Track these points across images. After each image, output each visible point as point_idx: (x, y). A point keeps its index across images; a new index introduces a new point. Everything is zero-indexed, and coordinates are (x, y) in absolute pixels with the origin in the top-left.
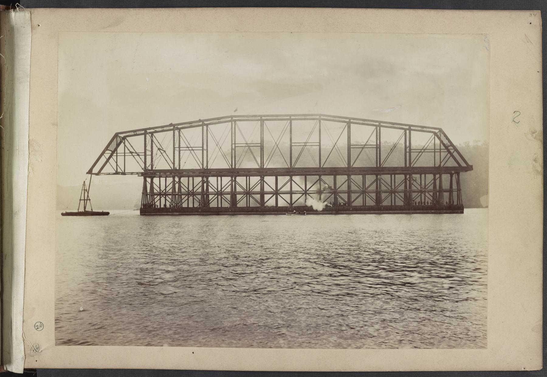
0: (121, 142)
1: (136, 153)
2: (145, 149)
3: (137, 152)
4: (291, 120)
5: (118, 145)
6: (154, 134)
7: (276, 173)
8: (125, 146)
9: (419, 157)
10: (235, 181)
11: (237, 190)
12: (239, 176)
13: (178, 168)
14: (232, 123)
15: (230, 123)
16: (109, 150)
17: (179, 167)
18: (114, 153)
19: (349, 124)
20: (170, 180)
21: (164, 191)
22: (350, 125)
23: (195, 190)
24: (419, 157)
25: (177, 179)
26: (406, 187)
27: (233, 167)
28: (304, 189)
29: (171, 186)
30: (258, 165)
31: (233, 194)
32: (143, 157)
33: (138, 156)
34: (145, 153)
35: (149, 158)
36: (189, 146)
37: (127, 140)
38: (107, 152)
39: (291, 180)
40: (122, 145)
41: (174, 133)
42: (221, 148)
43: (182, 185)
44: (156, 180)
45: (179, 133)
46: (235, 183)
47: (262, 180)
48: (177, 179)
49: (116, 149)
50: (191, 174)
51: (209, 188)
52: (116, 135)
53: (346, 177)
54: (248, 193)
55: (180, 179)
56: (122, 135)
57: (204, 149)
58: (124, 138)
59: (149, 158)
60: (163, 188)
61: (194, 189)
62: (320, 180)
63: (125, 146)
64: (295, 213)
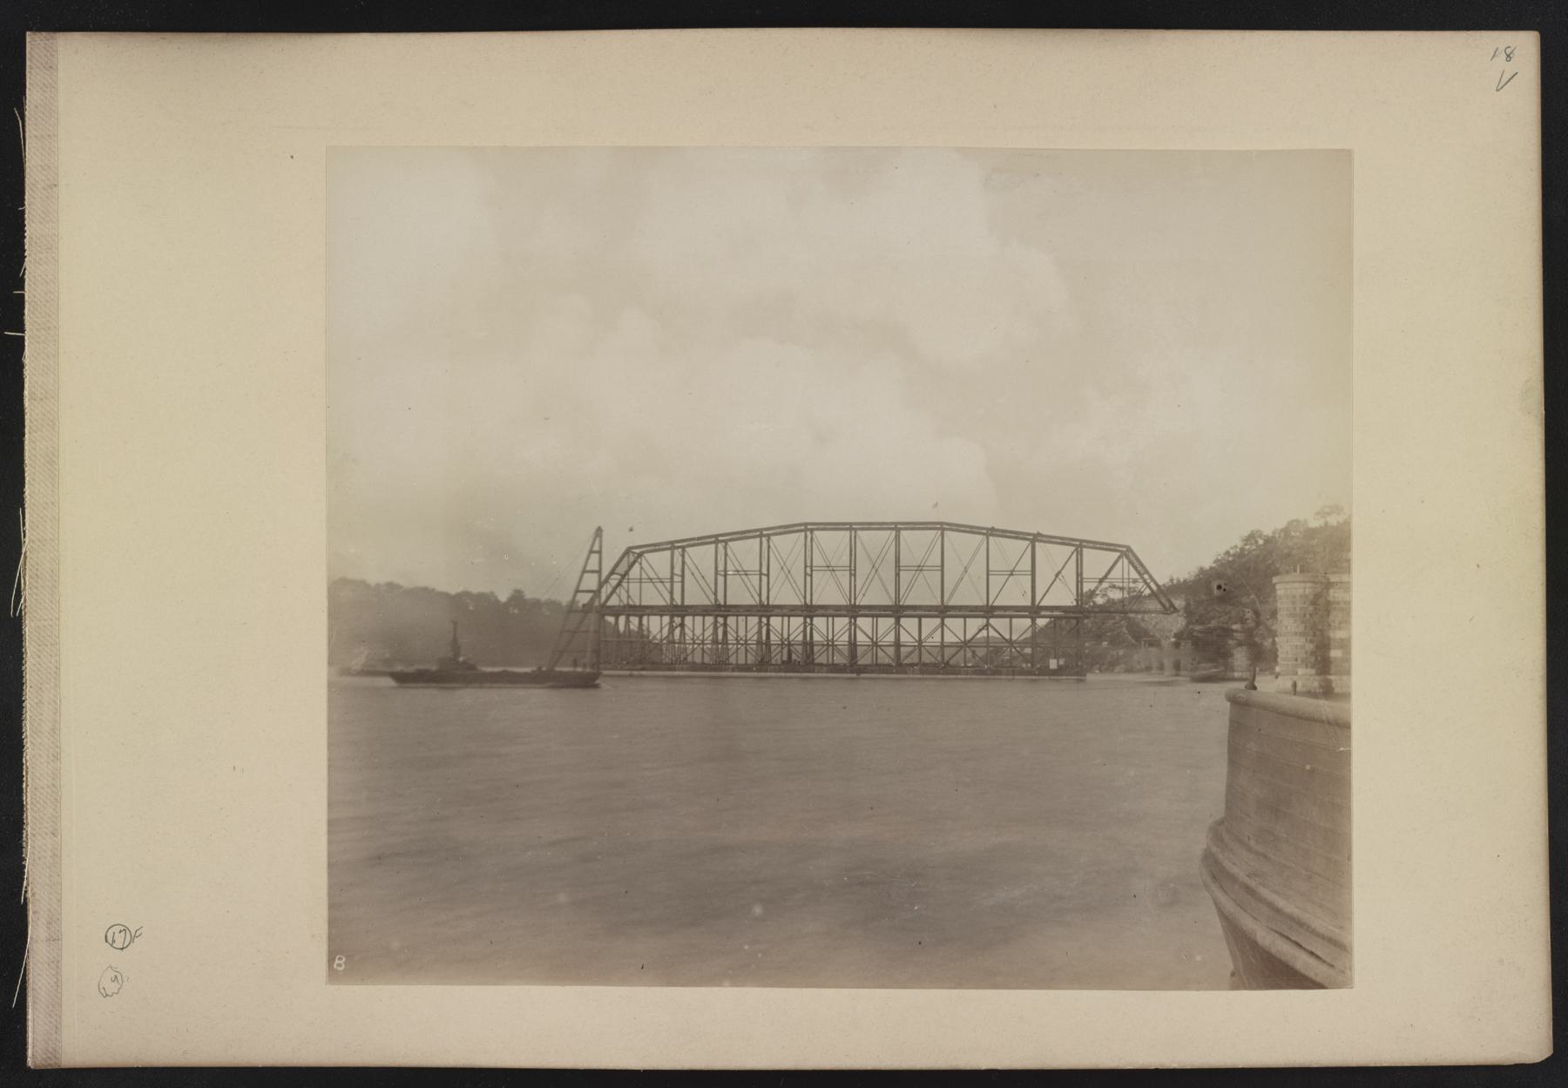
0: (634, 562)
1: (659, 578)
2: (672, 574)
3: (660, 577)
4: (898, 530)
5: (631, 566)
6: (687, 549)
7: (875, 612)
8: (642, 568)
9: (737, 560)
10: (855, 624)
11: (858, 639)
12: (992, 617)
13: (722, 603)
14: (806, 534)
15: (803, 534)
16: (617, 574)
17: (768, 602)
18: (1111, 602)
19: (1033, 543)
20: (666, 619)
21: (701, 638)
22: (1081, 551)
23: (791, 638)
24: (737, 560)
25: (764, 620)
26: (805, 636)
27: (853, 602)
28: (917, 638)
29: (756, 629)
30: (890, 597)
31: (853, 645)
32: (668, 585)
33: (661, 584)
34: (672, 578)
35: (677, 587)
36: (740, 569)
37: (646, 560)
38: (614, 576)
39: (943, 624)
40: (637, 565)
41: (716, 548)
42: (782, 568)
43: (771, 628)
44: (688, 620)
45: (725, 548)
46: (855, 628)
47: (898, 622)
48: (764, 620)
49: (627, 573)
50: (785, 611)
51: (771, 633)
52: (628, 551)
53: (892, 621)
54: (830, 645)
55: (768, 621)
56: (638, 551)
57: (766, 574)
58: (640, 555)
59: (677, 587)
60: (742, 633)
61: (706, 633)
62: (987, 625)
63: (642, 568)
64: (1060, 671)
